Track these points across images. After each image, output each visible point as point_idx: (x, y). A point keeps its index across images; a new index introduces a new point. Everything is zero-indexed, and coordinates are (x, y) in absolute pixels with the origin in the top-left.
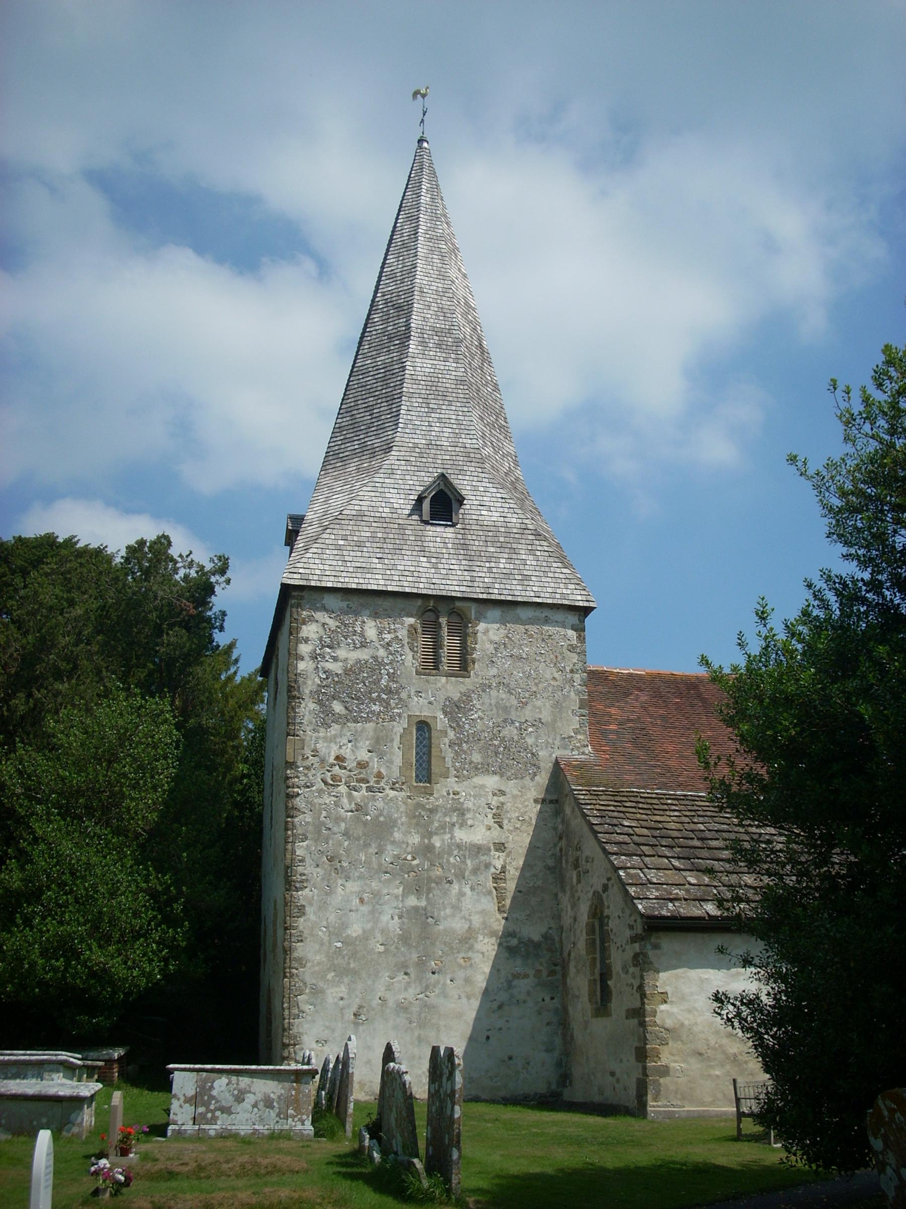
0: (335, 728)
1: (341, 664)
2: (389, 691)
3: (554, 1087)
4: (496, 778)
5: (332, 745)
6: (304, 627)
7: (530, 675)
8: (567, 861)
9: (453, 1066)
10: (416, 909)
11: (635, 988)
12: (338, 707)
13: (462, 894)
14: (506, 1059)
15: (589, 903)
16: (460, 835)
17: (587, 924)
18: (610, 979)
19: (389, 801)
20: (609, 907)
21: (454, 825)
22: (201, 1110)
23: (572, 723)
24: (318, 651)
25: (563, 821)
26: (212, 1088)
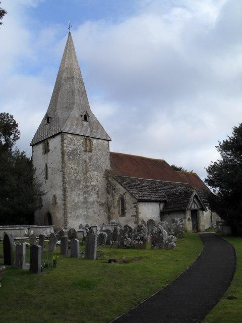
0: (71, 162)
2: (79, 154)
9: (21, 255)
12: (71, 157)
16: (92, 183)
23: (108, 162)
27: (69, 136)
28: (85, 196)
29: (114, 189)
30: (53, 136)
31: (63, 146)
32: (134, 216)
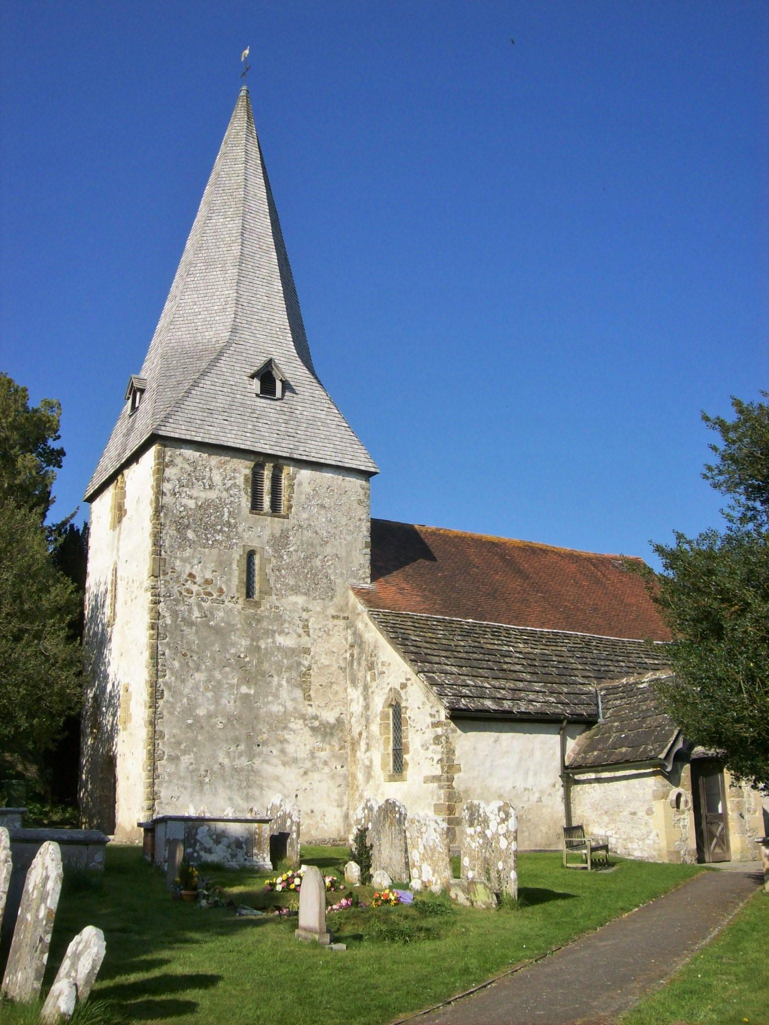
0: (188, 552)
1: (194, 501)
3: (342, 833)
4: (305, 598)
5: (187, 564)
6: (166, 469)
7: (331, 521)
8: (359, 664)
10: (247, 696)
11: (435, 761)
12: (190, 534)
13: (280, 685)
14: (309, 812)
15: (385, 697)
16: (280, 639)
17: (382, 712)
18: (407, 752)
19: (229, 612)
20: (407, 700)
21: (275, 632)
22: (190, 850)
24: (176, 490)
25: (354, 633)
26: (196, 834)
27: (189, 453)
28: (244, 689)
29: (371, 667)
30: (135, 458)
31: (159, 493)
32: (435, 779)
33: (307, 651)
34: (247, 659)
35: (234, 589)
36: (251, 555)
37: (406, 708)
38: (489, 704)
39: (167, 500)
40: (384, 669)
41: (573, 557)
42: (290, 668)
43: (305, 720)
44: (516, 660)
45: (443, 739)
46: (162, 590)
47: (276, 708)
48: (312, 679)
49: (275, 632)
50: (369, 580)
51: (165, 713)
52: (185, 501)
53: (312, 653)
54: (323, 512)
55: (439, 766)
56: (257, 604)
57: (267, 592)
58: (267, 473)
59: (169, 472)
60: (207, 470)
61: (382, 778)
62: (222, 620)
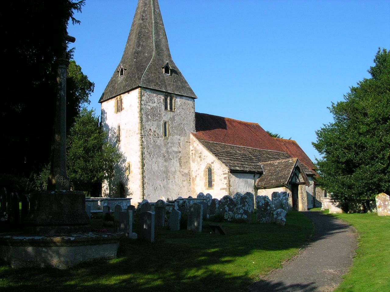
4: (179, 136)
11: (225, 184)
21: (172, 146)
29: (200, 157)
33: (180, 152)
34: (165, 155)
35: (161, 134)
36: (165, 123)
37: (214, 169)
38: (238, 168)
39: (143, 106)
40: (205, 158)
41: (241, 123)
42: (176, 157)
43: (180, 172)
44: (238, 156)
45: (227, 178)
46: (143, 134)
47: (173, 169)
48: (182, 160)
49: (172, 146)
50: (195, 131)
51: (146, 170)
52: (147, 107)
53: (181, 153)
54: (183, 110)
55: (226, 185)
56: (167, 139)
57: (169, 135)
58: (169, 98)
59: (143, 98)
60: (153, 97)
61: (205, 189)
62: (159, 143)
